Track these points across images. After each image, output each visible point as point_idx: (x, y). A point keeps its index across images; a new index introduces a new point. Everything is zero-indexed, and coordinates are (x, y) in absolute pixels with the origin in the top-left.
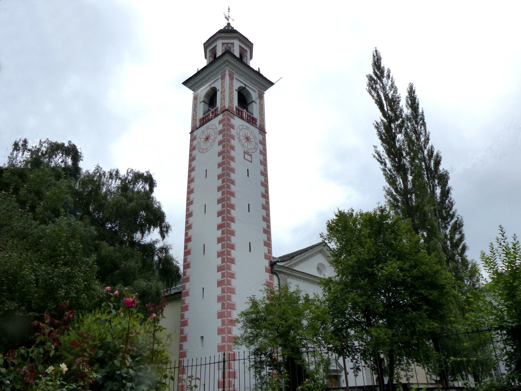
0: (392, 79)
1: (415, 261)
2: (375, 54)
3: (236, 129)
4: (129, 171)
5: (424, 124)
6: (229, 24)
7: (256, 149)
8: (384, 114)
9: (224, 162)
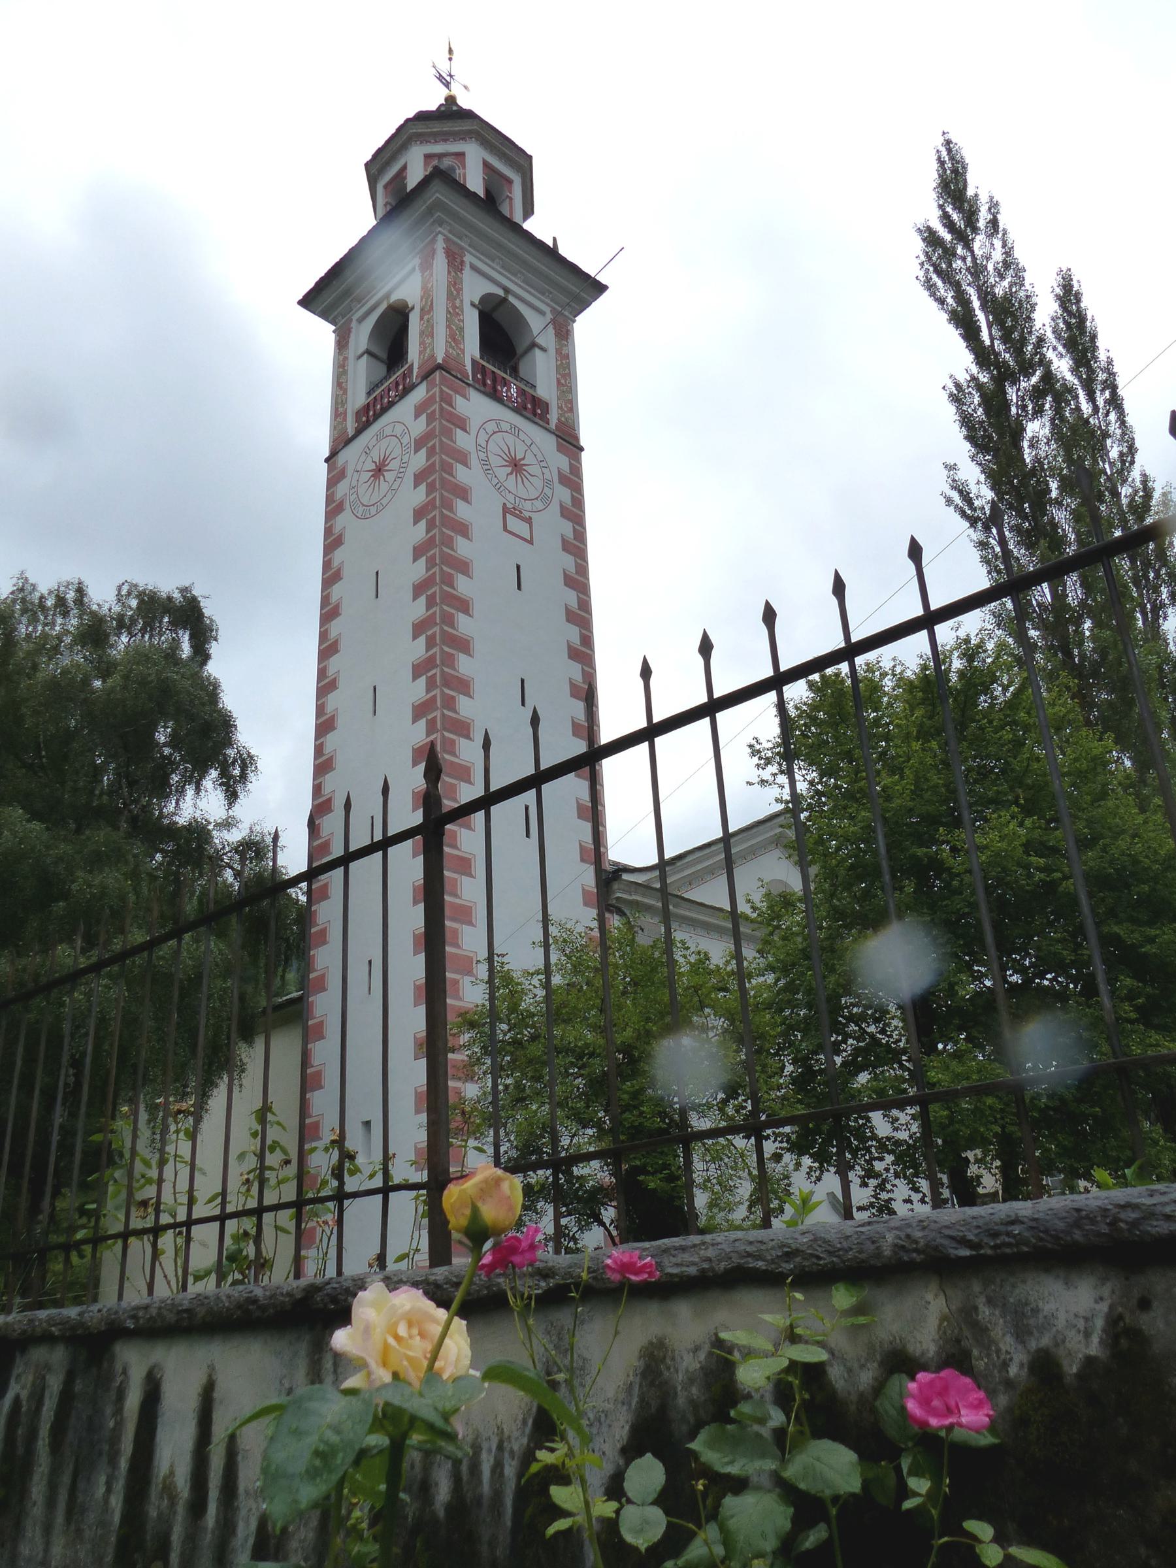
0: (1005, 233)
1: (1090, 822)
2: (944, 153)
3: (473, 432)
4: (124, 592)
5: (1115, 402)
6: (451, 100)
7: (547, 501)
8: (983, 356)
9: (432, 539)
